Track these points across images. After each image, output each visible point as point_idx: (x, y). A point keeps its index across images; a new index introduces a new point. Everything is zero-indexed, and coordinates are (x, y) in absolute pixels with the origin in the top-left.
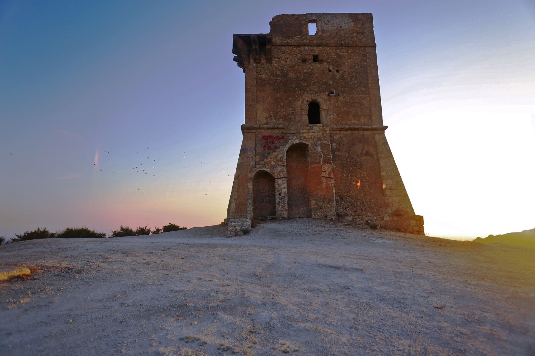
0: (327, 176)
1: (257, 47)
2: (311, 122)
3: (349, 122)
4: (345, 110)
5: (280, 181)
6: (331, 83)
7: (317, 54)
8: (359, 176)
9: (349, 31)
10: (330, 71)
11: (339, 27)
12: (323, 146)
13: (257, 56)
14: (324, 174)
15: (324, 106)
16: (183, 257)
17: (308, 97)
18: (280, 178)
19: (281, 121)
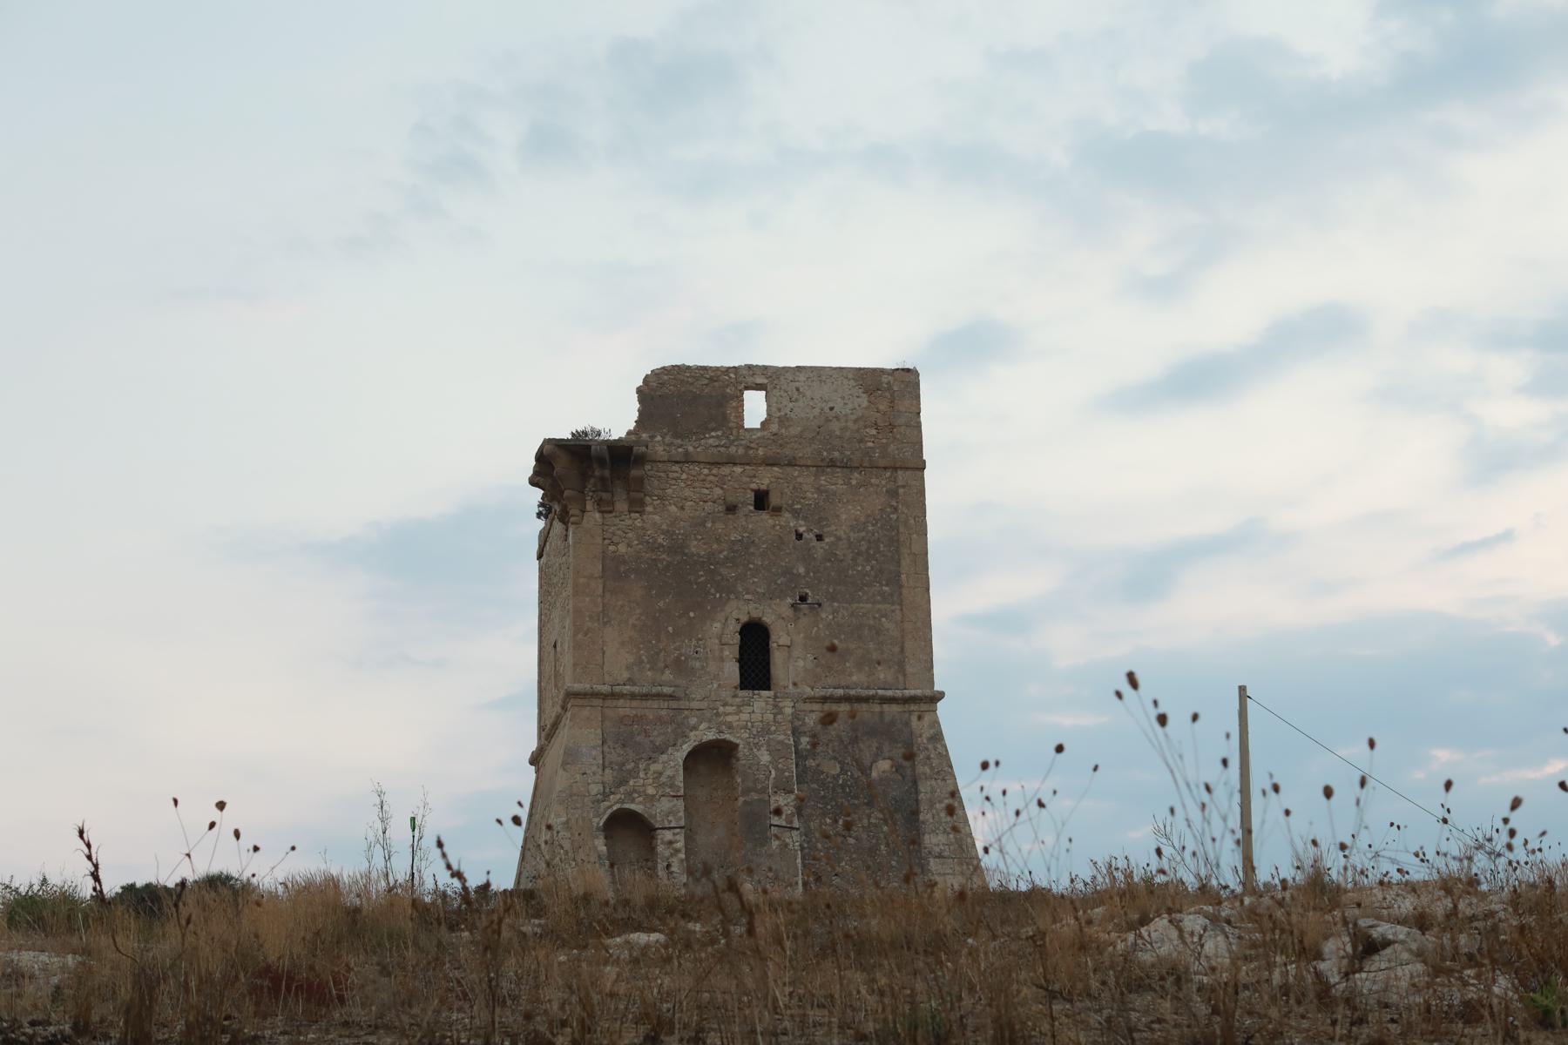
5: (668, 835)
6: (802, 570)
7: (763, 487)
9: (855, 421)
10: (799, 536)
17: (738, 611)
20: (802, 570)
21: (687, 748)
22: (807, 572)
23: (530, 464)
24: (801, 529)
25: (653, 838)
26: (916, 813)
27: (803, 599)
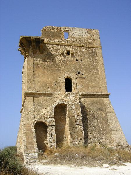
0: (79, 124)
1: (35, 44)
2: (67, 90)
3: (89, 91)
4: (86, 84)
5: (51, 128)
6: (78, 67)
7: (69, 50)
8: (96, 123)
9: (87, 38)
10: (77, 60)
11: (81, 36)
12: (75, 105)
13: (34, 50)
14: (77, 123)
15: (74, 81)
16: (106, 115)
17: (66, 75)
18: (51, 126)
19: (49, 89)
20: (78, 67)
21: (55, 105)
22: (79, 67)
23: (19, 44)
24: (77, 59)
25: (47, 128)
26: (107, 120)
27: (79, 73)
